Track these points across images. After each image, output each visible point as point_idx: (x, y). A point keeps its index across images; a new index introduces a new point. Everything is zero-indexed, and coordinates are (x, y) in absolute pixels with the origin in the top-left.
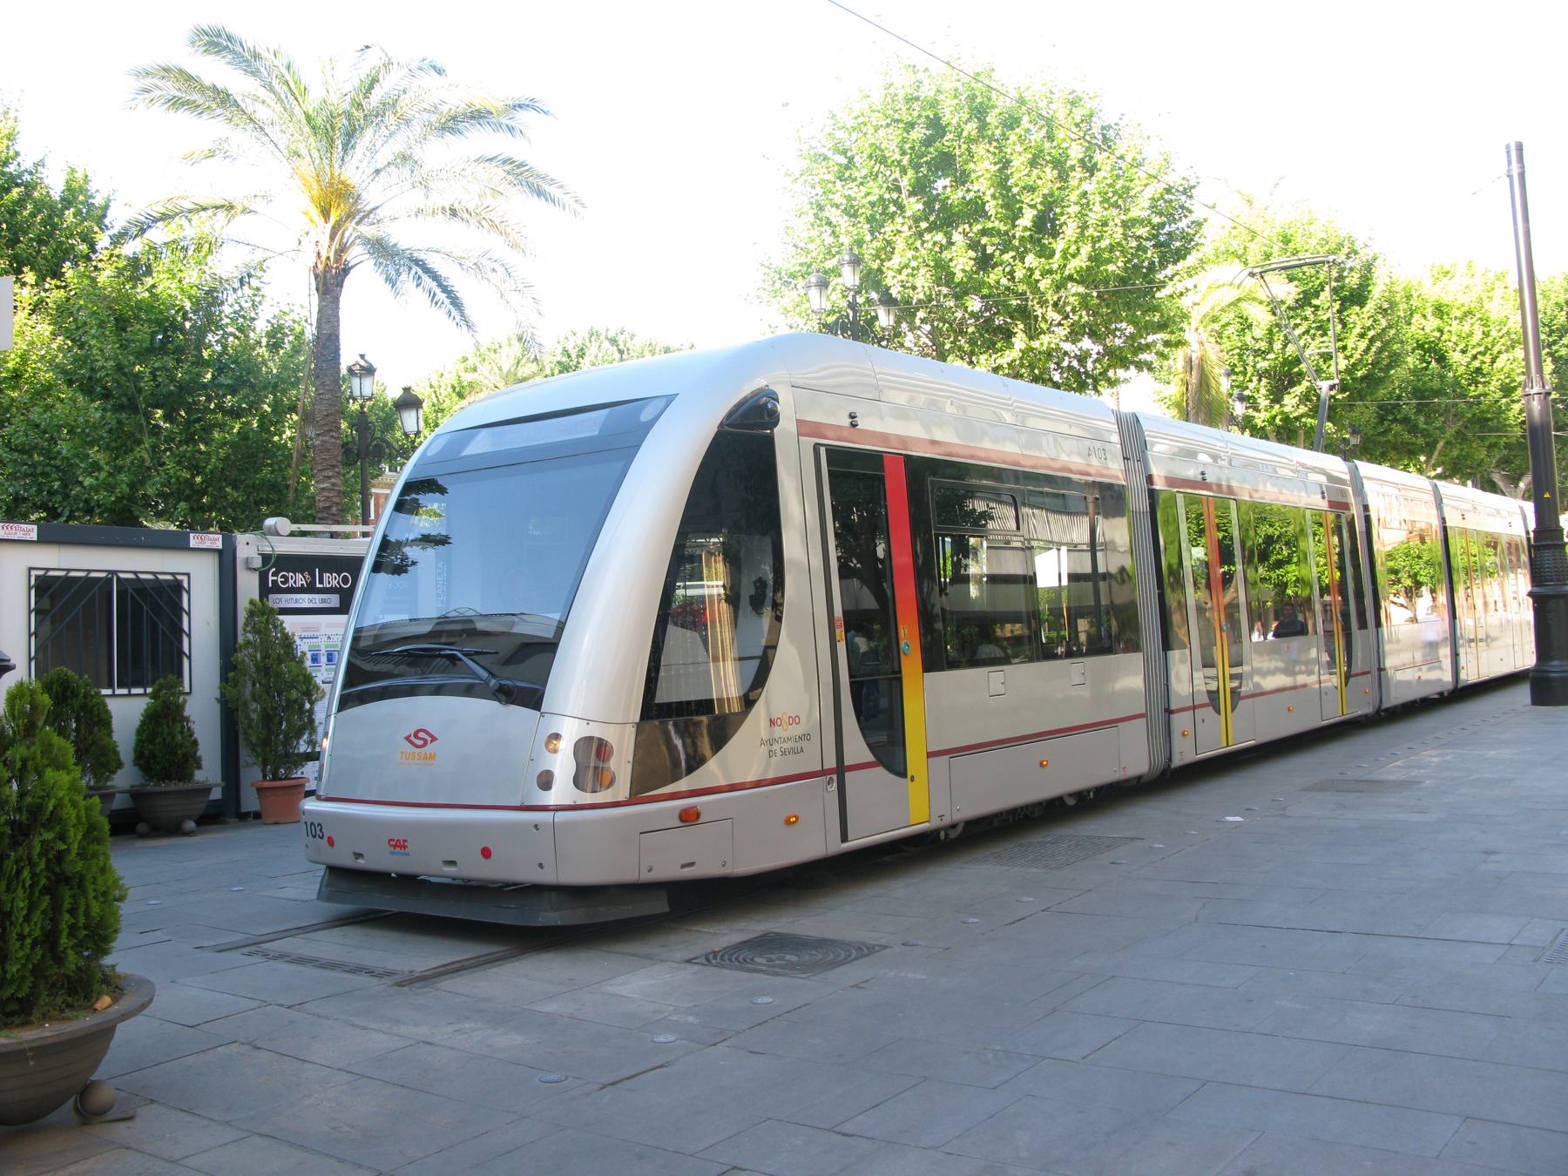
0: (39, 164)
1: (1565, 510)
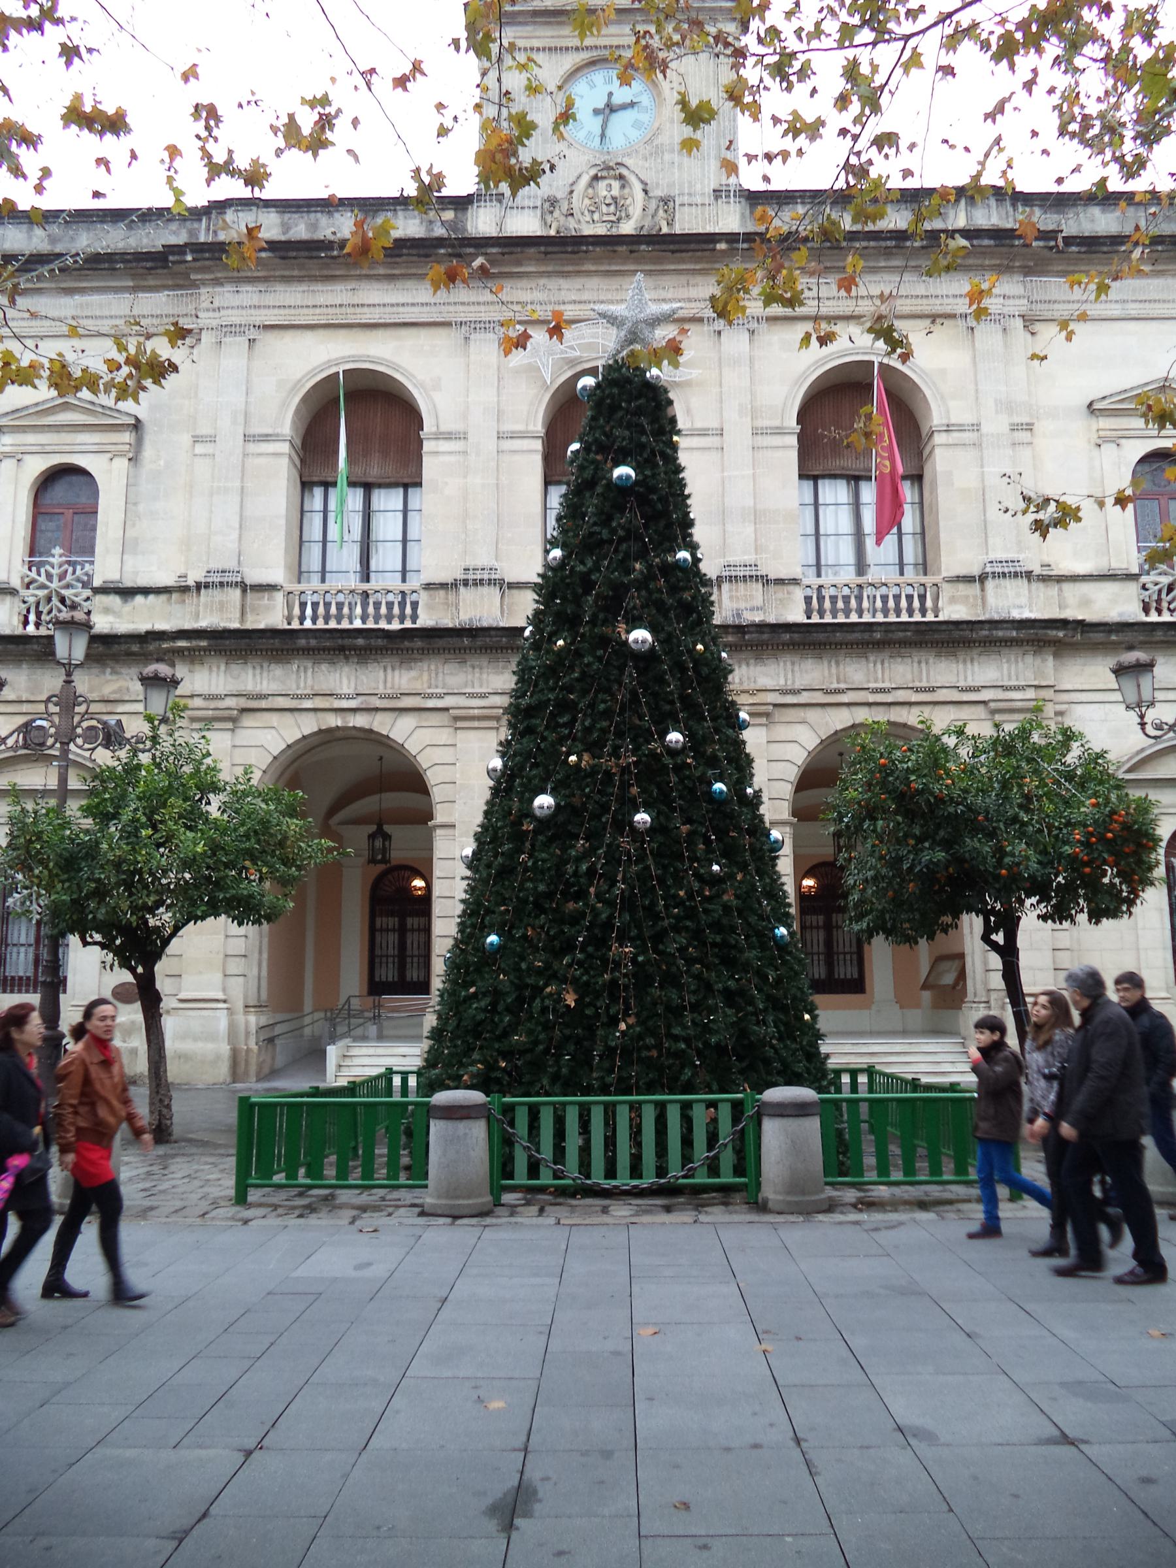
0: (551, 338)
1: (1172, 1075)
